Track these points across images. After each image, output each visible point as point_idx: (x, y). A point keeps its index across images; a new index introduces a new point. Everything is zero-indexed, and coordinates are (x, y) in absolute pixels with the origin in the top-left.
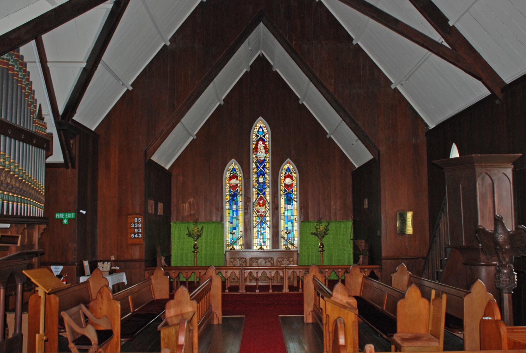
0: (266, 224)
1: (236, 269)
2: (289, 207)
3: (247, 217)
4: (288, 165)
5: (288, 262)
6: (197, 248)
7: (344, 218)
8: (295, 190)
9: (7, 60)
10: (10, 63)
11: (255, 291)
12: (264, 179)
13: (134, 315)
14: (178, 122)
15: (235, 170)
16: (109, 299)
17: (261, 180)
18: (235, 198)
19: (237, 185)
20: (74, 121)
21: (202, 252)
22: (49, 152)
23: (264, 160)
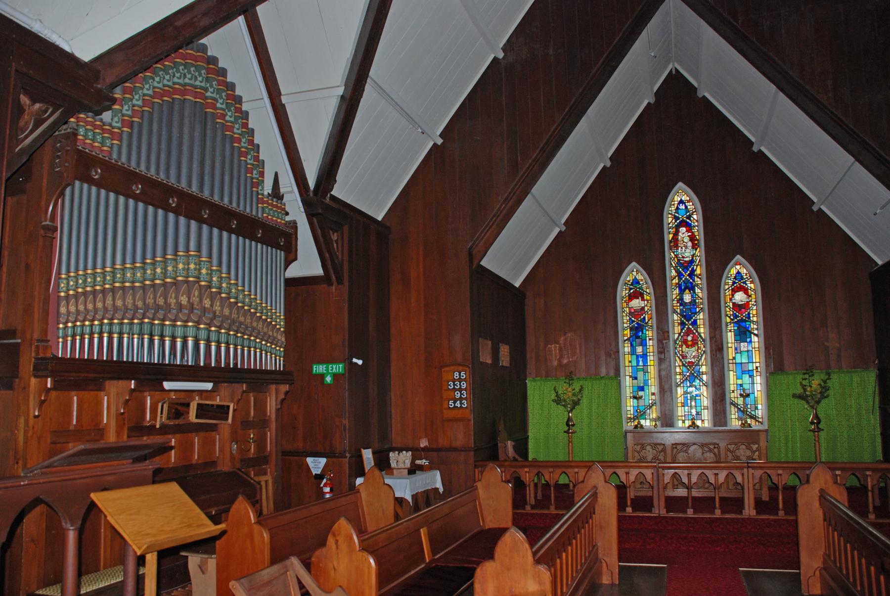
0: (701, 380)
1: (647, 467)
2: (744, 346)
3: (663, 366)
4: (739, 268)
5: (749, 453)
6: (573, 425)
7: (859, 363)
8: (755, 313)
9: (201, 88)
10: (208, 94)
11: (686, 512)
12: (692, 296)
13: (429, 571)
14: (526, 193)
15: (638, 283)
16: (351, 550)
17: (687, 298)
18: (640, 334)
19: (643, 308)
20: (333, 198)
21: (582, 430)
22: (291, 257)
23: (692, 261)
